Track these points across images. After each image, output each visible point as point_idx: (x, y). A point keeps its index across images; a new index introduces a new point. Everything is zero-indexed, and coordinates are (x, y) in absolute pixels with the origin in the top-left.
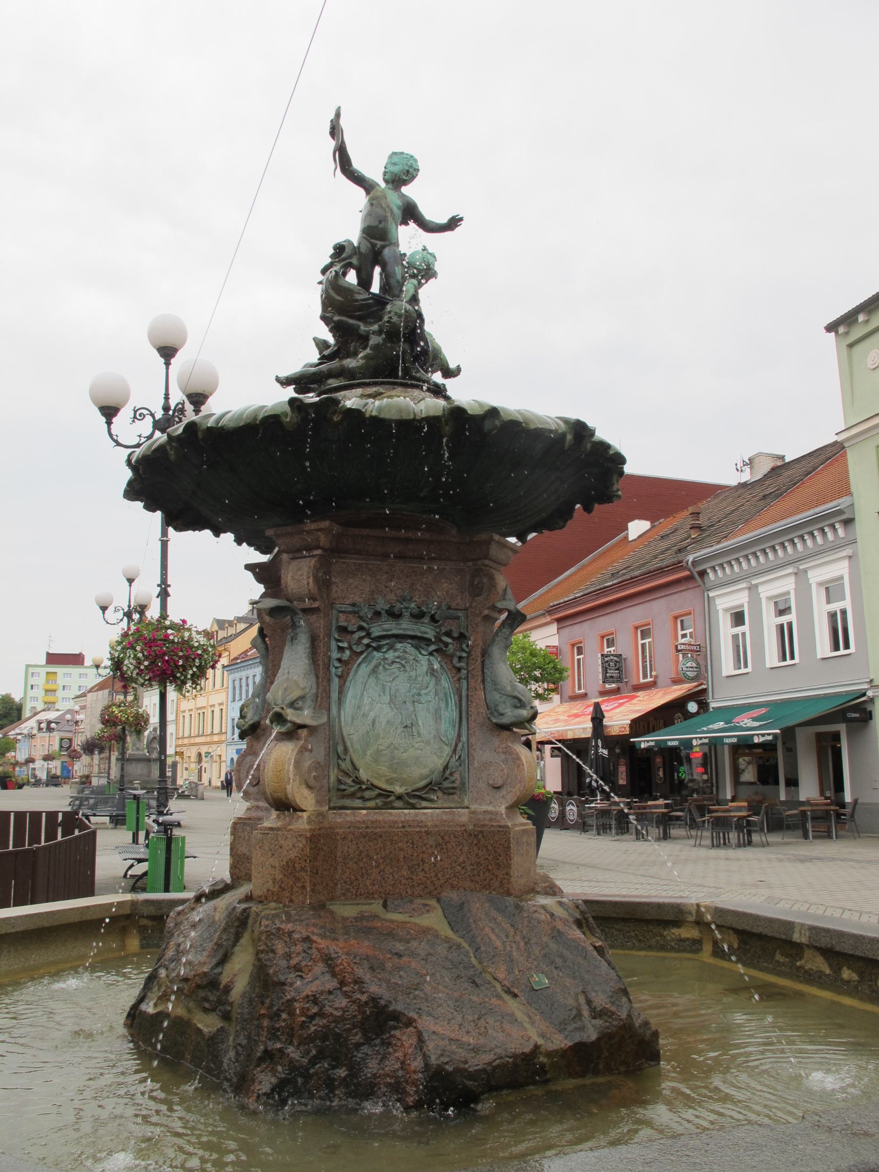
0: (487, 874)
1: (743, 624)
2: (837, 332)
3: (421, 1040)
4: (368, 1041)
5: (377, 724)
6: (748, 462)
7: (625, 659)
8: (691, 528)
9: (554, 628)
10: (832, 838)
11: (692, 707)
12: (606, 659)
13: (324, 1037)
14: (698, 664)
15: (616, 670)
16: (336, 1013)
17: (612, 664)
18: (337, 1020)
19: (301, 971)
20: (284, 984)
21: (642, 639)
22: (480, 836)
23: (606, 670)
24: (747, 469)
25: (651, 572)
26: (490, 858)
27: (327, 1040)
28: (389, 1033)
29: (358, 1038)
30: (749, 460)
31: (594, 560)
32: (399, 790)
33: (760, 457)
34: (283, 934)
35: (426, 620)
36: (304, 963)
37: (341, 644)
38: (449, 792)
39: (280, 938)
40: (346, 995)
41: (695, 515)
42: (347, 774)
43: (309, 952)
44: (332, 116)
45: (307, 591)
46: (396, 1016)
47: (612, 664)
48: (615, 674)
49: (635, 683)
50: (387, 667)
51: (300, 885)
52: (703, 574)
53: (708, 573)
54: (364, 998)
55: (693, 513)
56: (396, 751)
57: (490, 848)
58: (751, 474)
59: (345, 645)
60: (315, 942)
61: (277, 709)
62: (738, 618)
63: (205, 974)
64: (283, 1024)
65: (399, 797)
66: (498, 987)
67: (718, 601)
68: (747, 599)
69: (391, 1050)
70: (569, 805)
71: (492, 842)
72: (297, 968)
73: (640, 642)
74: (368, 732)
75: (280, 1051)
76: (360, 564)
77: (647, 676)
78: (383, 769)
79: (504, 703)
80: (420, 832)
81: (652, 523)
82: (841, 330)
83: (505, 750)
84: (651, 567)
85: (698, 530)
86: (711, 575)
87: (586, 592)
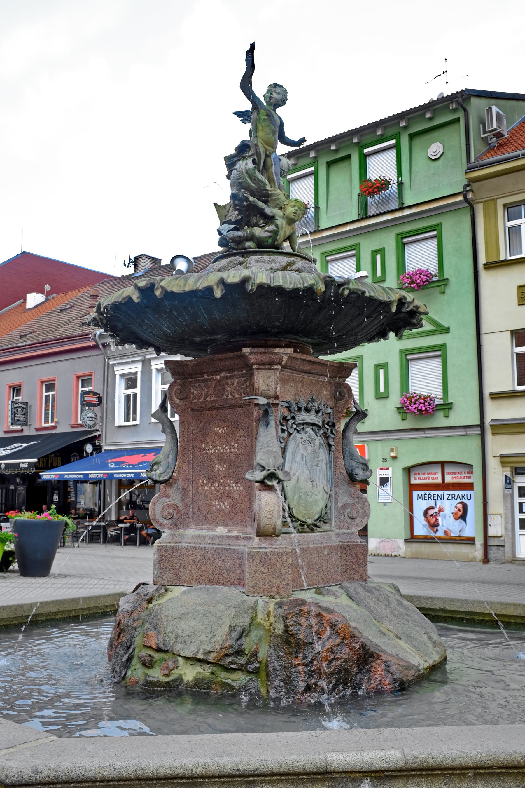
0: (352, 571)
1: (135, 387)
4: (360, 671)
5: (300, 480)
6: (134, 260)
7: (30, 407)
10: (121, 545)
11: (89, 448)
12: (15, 406)
14: (96, 415)
15: (22, 415)
16: (344, 657)
17: (20, 410)
19: (320, 634)
20: (312, 643)
21: (46, 391)
22: (348, 548)
23: (15, 415)
26: (354, 561)
27: (341, 674)
28: (370, 664)
29: (355, 670)
32: (310, 521)
34: (304, 613)
35: (303, 412)
36: (320, 630)
37: (283, 427)
39: (301, 616)
40: (346, 645)
41: (94, 297)
43: (321, 622)
44: (248, 47)
45: (273, 393)
46: (372, 655)
47: (20, 410)
49: (38, 426)
50: (304, 443)
51: (285, 583)
53: (110, 346)
54: (357, 646)
55: (93, 296)
56: (308, 497)
57: (354, 555)
59: (285, 428)
60: (324, 616)
61: (272, 470)
62: (131, 382)
63: (231, 647)
64: (316, 668)
66: (392, 635)
67: (116, 368)
68: (140, 369)
69: (372, 674)
71: (355, 552)
73: (45, 394)
74: (295, 485)
75: (316, 684)
76: (290, 376)
77: (48, 422)
79: (358, 468)
80: (321, 547)
83: (358, 496)
84: (56, 334)
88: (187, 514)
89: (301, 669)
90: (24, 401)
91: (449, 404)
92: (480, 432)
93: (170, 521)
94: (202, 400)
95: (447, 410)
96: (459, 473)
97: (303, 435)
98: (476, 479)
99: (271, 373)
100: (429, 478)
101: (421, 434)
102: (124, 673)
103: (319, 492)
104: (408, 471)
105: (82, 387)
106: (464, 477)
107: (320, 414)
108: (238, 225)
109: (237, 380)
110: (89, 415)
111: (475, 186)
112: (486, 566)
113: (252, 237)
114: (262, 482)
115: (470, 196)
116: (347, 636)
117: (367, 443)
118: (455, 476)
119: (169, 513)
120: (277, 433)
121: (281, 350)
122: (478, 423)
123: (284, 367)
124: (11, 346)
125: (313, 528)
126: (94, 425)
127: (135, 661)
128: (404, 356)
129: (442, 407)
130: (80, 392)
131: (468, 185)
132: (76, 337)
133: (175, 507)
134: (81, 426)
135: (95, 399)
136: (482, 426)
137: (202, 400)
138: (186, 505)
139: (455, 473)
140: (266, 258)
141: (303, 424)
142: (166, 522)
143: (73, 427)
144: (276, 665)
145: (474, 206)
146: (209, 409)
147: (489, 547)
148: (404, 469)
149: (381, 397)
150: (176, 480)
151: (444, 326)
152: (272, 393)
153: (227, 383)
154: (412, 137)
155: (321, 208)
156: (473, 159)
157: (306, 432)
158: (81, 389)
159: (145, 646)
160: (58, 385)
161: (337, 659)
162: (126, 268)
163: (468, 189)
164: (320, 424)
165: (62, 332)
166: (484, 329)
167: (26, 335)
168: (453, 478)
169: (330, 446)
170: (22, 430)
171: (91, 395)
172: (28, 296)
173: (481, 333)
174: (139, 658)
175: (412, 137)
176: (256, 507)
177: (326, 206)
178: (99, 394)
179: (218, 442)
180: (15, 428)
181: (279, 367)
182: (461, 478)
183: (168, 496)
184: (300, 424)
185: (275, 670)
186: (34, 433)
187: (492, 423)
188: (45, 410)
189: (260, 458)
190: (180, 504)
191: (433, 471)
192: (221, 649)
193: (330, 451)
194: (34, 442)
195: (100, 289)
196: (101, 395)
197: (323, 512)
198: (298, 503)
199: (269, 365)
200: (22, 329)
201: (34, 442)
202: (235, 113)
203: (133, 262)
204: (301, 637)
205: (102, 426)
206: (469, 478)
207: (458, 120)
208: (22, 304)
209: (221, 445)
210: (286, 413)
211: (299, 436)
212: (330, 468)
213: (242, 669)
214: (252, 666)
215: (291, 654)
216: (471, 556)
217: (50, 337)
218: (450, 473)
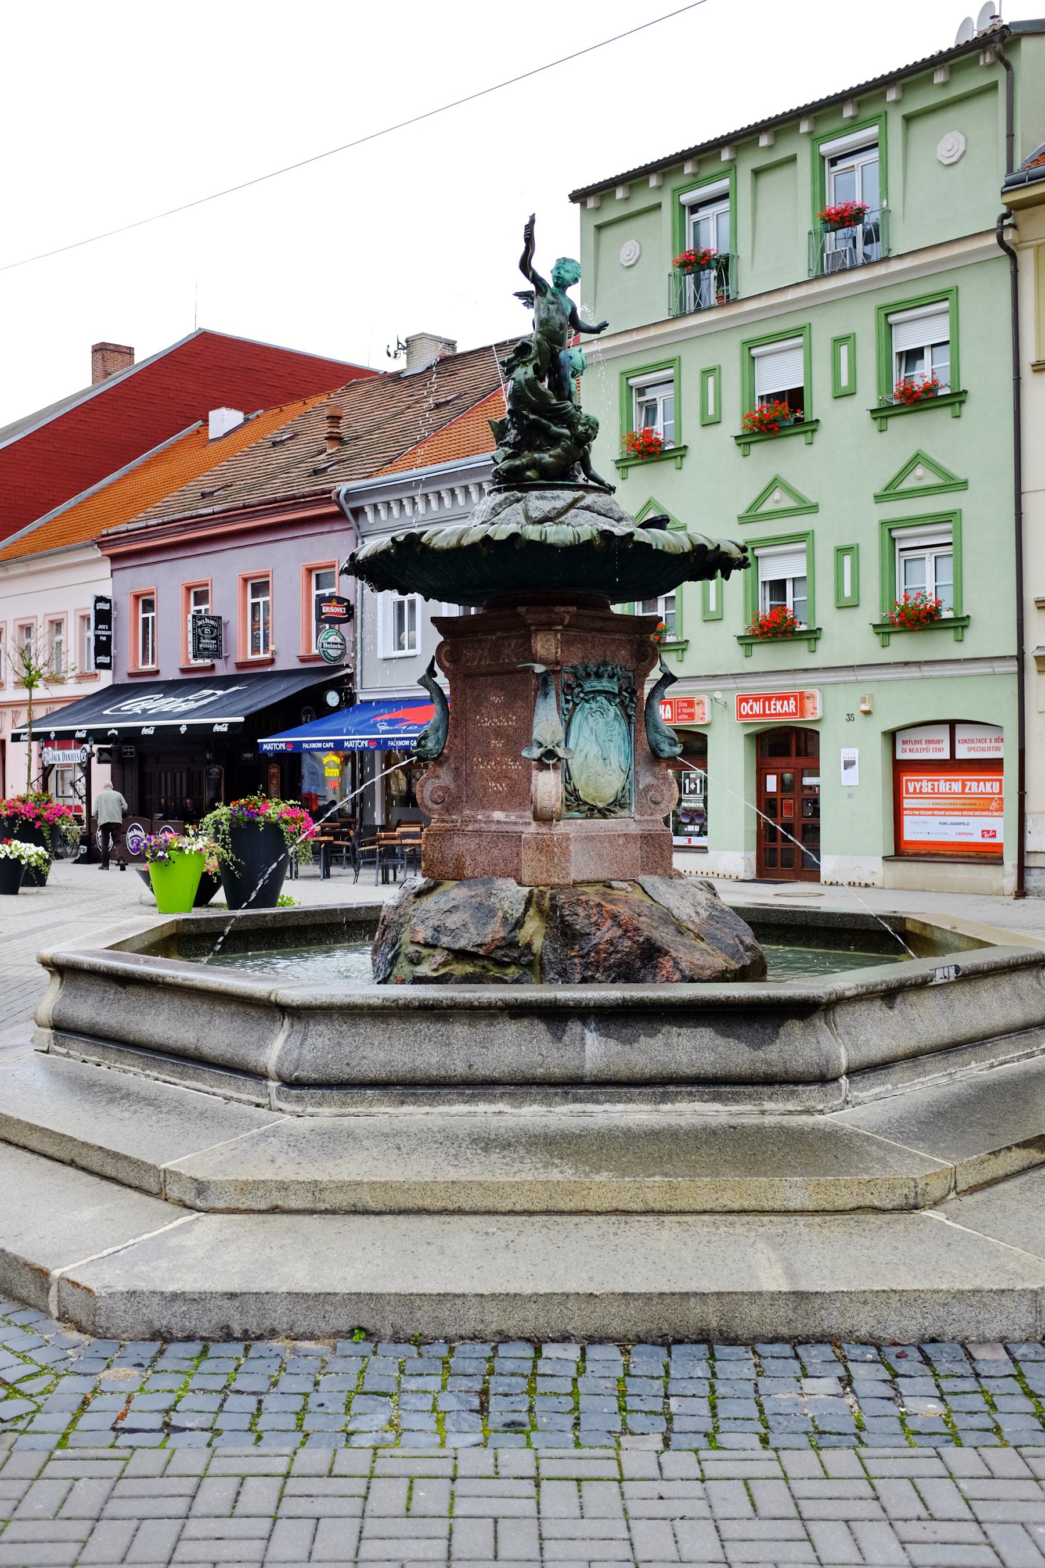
2: (584, 204)
3: (676, 963)
4: (644, 966)
6: (405, 344)
7: (226, 624)
8: (326, 439)
9: (107, 566)
11: (333, 699)
12: (200, 623)
13: (619, 965)
15: (212, 639)
18: (627, 954)
20: (589, 934)
24: (403, 356)
25: (276, 501)
29: (638, 964)
30: (407, 341)
31: (148, 464)
32: (601, 805)
33: (424, 340)
38: (622, 806)
39: (579, 905)
40: (629, 937)
42: (572, 795)
48: (211, 644)
49: (240, 659)
52: (358, 512)
54: (641, 939)
58: (408, 362)
59: (569, 698)
61: (550, 747)
63: (503, 938)
65: (600, 811)
70: (132, 829)
72: (596, 924)
73: (251, 601)
78: (591, 791)
81: (245, 414)
82: (591, 203)
85: (337, 442)
86: (370, 516)
87: (166, 519)
88: (460, 797)
89: (577, 961)
90: (215, 614)
91: (963, 619)
92: (1016, 669)
93: (440, 806)
94: (475, 663)
95: (960, 629)
96: (980, 741)
97: (594, 705)
98: (1008, 754)
99: (551, 637)
100: (928, 750)
101: (913, 672)
102: (389, 971)
103: (614, 771)
104: (892, 736)
105: (318, 588)
106: (989, 749)
107: (615, 680)
108: (518, 449)
109: (514, 642)
110: (332, 639)
111: (1020, 216)
112: (1021, 901)
113: (534, 465)
114: (539, 760)
115: (1009, 236)
116: (630, 928)
117: (821, 687)
118: (972, 745)
119: (439, 796)
120: (558, 705)
121: (563, 609)
122: (1014, 652)
123: (567, 627)
124: (187, 514)
125: (604, 813)
126: (341, 657)
127: (401, 958)
128: (887, 532)
129: (952, 625)
130: (314, 598)
131: (1005, 216)
132: (304, 497)
133: (446, 790)
134: (317, 658)
135: (341, 610)
136: (1020, 658)
137: (475, 663)
138: (458, 787)
139: (973, 741)
140: (548, 493)
141: (593, 692)
142: (435, 806)
143: (303, 660)
144: (551, 957)
145: (1017, 254)
146: (484, 675)
147: (1027, 872)
148: (884, 733)
149: (846, 605)
150: (447, 758)
151: (958, 478)
152: (552, 657)
153: (503, 645)
154: (908, 119)
155: (742, 256)
156: (1018, 165)
157: (597, 702)
158: (315, 592)
159: (413, 942)
160: (275, 585)
161: (618, 952)
162: (391, 359)
163: (1006, 222)
164: (616, 691)
165: (276, 489)
166: (1026, 486)
167: (212, 493)
168: (970, 749)
169: (629, 717)
170: (213, 667)
171: (334, 603)
172: (212, 414)
173: (1023, 490)
174: (406, 955)
175: (908, 119)
176: (533, 788)
177: (750, 253)
178: (348, 601)
179: (494, 714)
180: (201, 662)
181: (560, 627)
182: (983, 749)
183: (438, 777)
184: (590, 692)
185: (550, 962)
186: (231, 670)
187: (1038, 653)
188: (253, 630)
189: (537, 734)
190: (452, 786)
191: (936, 738)
192: (493, 940)
193: (629, 723)
194: (236, 688)
195: (346, 399)
196: (351, 603)
197: (620, 795)
198: (587, 784)
199: (547, 626)
200: (206, 481)
201: (236, 688)
202: (516, 294)
203: (404, 348)
204: (578, 927)
205: (355, 658)
206: (998, 749)
207: (993, 87)
208: (201, 430)
209: (498, 717)
210: (571, 681)
211: (587, 705)
212: (630, 743)
213: (515, 962)
214: (526, 959)
215: (566, 945)
216: (995, 886)
217: (254, 498)
218: (966, 741)
